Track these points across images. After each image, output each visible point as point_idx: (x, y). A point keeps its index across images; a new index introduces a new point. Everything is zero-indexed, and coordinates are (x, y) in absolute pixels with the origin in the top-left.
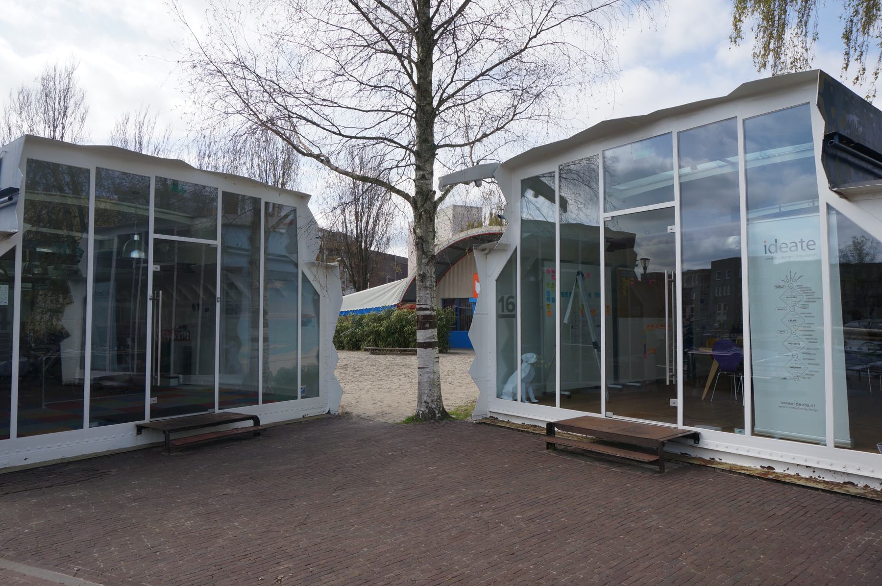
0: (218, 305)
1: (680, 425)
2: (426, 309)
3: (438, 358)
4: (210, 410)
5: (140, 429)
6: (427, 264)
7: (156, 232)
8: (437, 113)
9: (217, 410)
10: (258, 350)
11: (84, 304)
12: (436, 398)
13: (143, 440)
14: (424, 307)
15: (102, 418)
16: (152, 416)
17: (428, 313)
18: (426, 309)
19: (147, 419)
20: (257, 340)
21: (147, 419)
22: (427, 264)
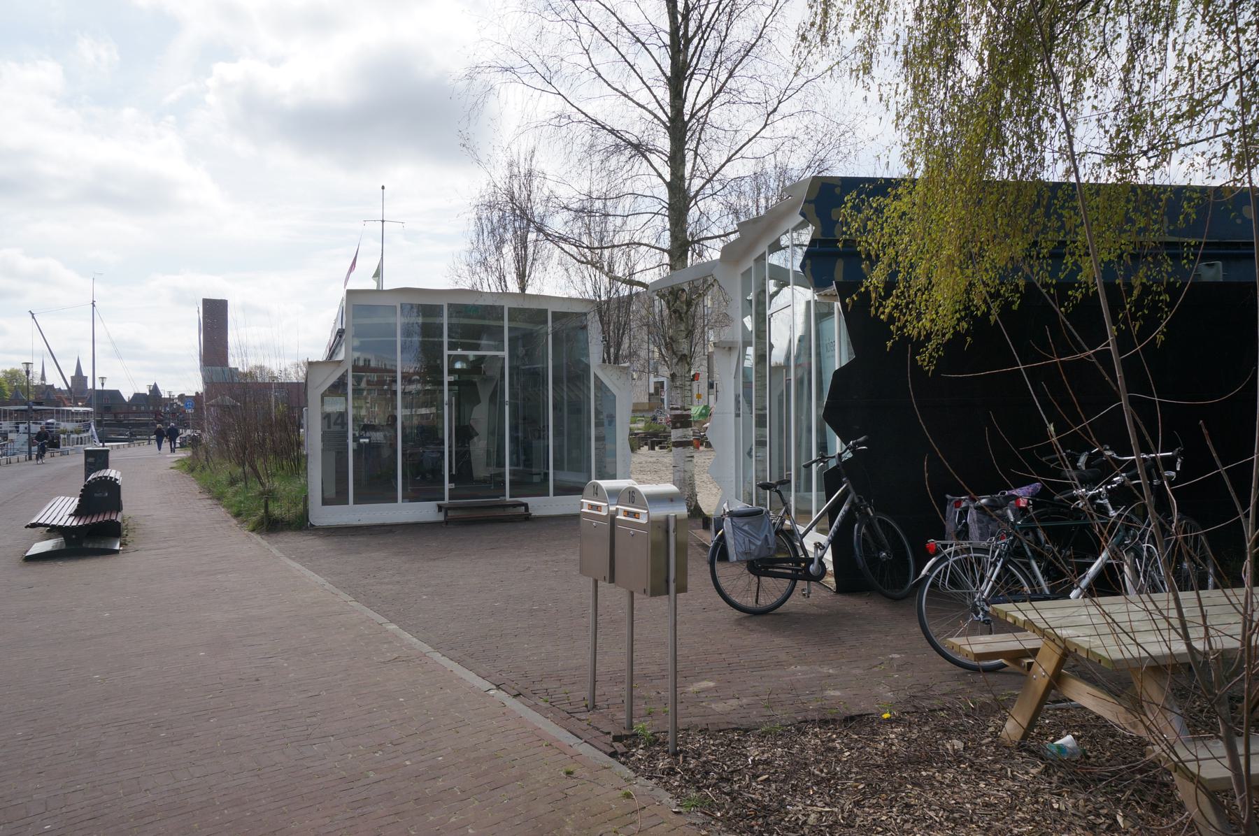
0: (507, 408)
1: (508, 498)
2: (677, 409)
3: (692, 457)
4: (502, 498)
5: (440, 508)
6: (677, 364)
7: (449, 349)
8: (1136, 56)
9: (508, 498)
10: (596, 449)
11: (821, 368)
12: (686, 496)
13: (441, 517)
14: (674, 406)
15: (411, 497)
16: (450, 499)
17: (678, 412)
18: (677, 409)
19: (447, 501)
20: (597, 439)
21: (447, 501)
22: (677, 364)
